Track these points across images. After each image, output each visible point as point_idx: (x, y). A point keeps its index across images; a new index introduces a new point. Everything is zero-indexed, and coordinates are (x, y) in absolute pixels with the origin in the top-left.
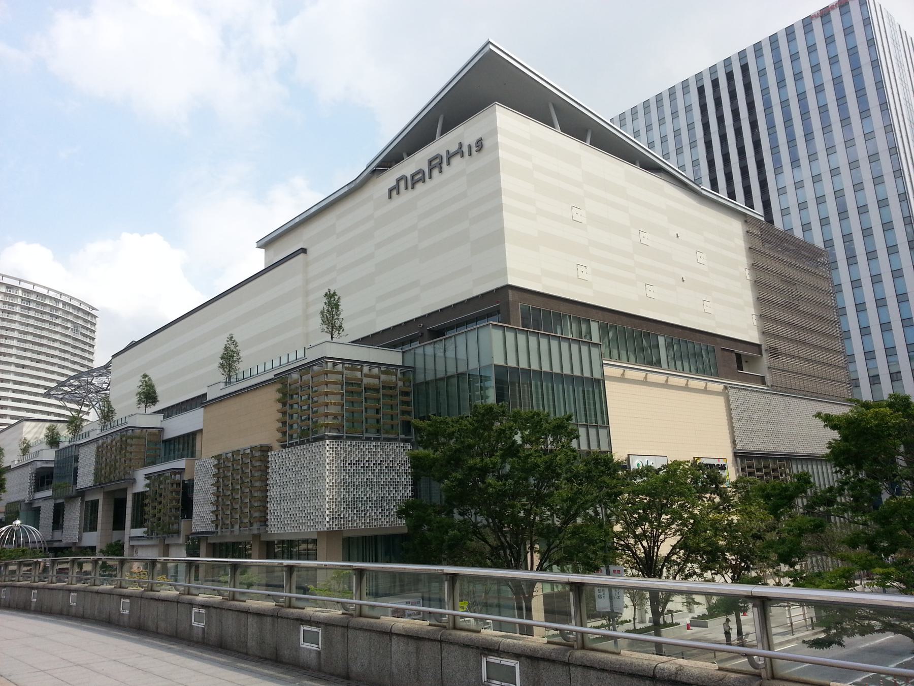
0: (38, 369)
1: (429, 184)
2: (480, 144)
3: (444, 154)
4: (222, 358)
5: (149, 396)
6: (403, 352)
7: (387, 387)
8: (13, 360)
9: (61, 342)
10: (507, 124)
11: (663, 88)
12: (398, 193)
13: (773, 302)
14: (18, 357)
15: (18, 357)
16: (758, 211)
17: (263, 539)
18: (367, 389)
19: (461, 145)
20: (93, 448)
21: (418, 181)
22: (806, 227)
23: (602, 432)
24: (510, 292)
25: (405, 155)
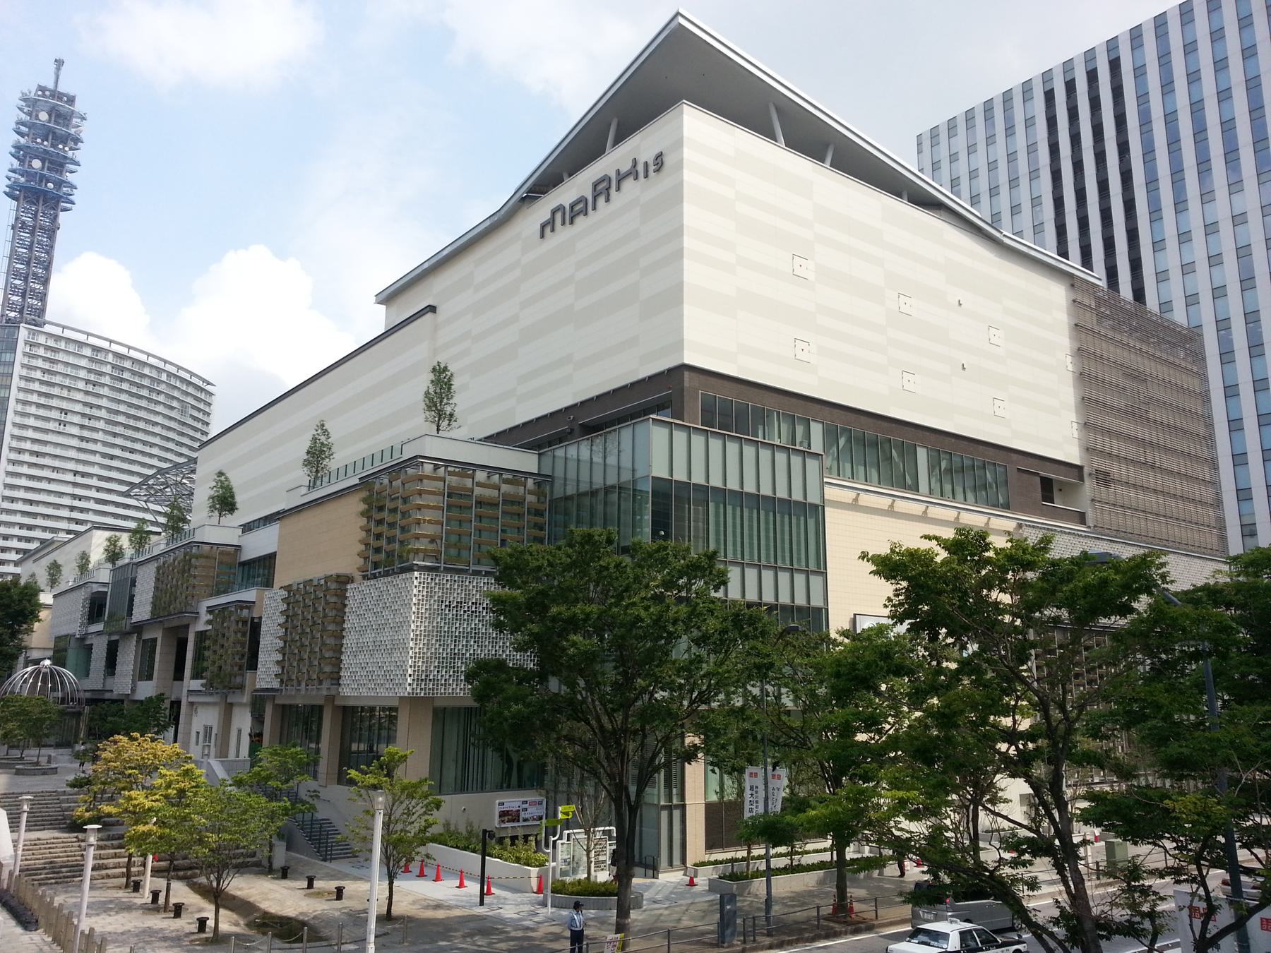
0: (132, 462)
2: (659, 160)
4: (308, 453)
5: (225, 502)
7: (508, 500)
9: (163, 426)
10: (698, 131)
11: (996, 92)
12: (553, 230)
13: (1106, 405)
14: (105, 444)
15: (105, 444)
16: (1098, 275)
18: (480, 503)
19: (635, 162)
20: (152, 567)
22: (1192, 300)
23: (816, 581)
24: (687, 374)
25: (565, 175)
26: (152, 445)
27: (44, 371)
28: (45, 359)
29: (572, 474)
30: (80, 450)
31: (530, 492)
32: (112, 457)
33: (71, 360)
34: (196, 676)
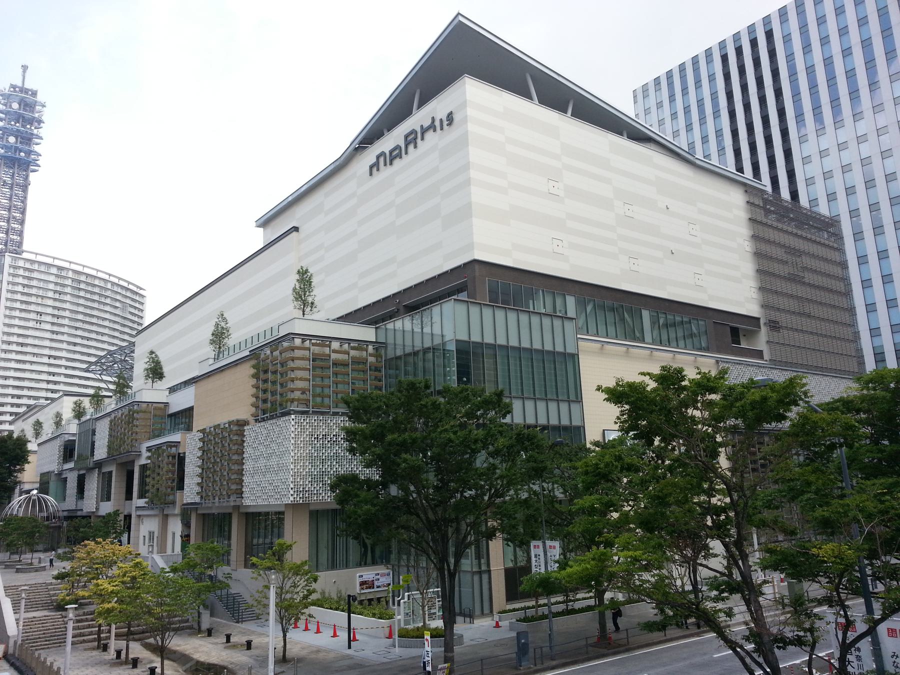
1: (406, 159)
2: (450, 118)
3: (419, 130)
4: (213, 334)
5: (156, 372)
6: (376, 328)
7: (356, 361)
8: (65, 338)
9: (110, 321)
10: (474, 96)
12: (378, 170)
17: (242, 510)
18: (335, 364)
19: (433, 119)
20: (107, 421)
21: (395, 157)
25: (385, 131)
26: (103, 334)
27: (24, 286)
28: (24, 277)
29: (399, 341)
30: (52, 340)
31: (371, 355)
32: (75, 344)
33: (43, 277)
34: (141, 496)
